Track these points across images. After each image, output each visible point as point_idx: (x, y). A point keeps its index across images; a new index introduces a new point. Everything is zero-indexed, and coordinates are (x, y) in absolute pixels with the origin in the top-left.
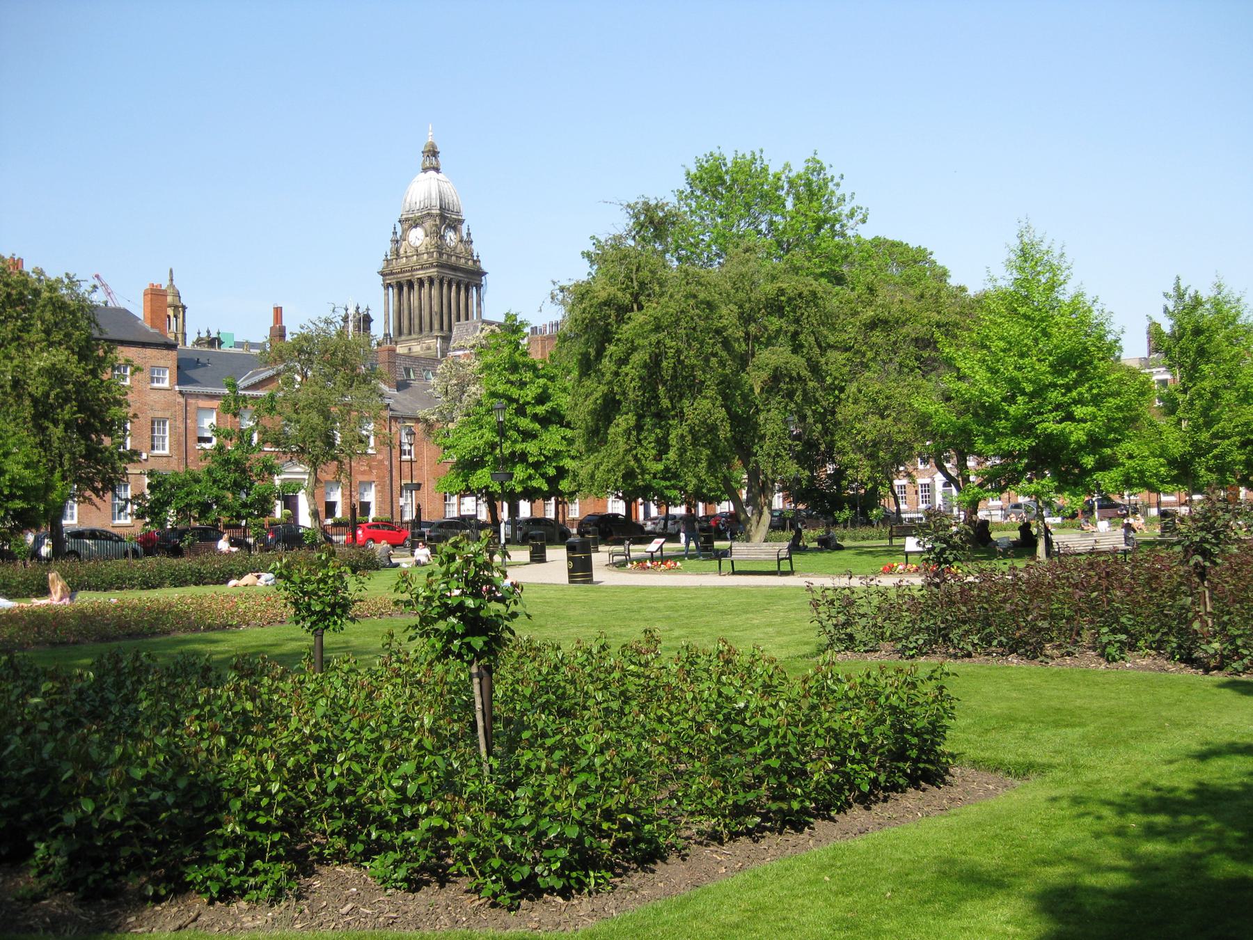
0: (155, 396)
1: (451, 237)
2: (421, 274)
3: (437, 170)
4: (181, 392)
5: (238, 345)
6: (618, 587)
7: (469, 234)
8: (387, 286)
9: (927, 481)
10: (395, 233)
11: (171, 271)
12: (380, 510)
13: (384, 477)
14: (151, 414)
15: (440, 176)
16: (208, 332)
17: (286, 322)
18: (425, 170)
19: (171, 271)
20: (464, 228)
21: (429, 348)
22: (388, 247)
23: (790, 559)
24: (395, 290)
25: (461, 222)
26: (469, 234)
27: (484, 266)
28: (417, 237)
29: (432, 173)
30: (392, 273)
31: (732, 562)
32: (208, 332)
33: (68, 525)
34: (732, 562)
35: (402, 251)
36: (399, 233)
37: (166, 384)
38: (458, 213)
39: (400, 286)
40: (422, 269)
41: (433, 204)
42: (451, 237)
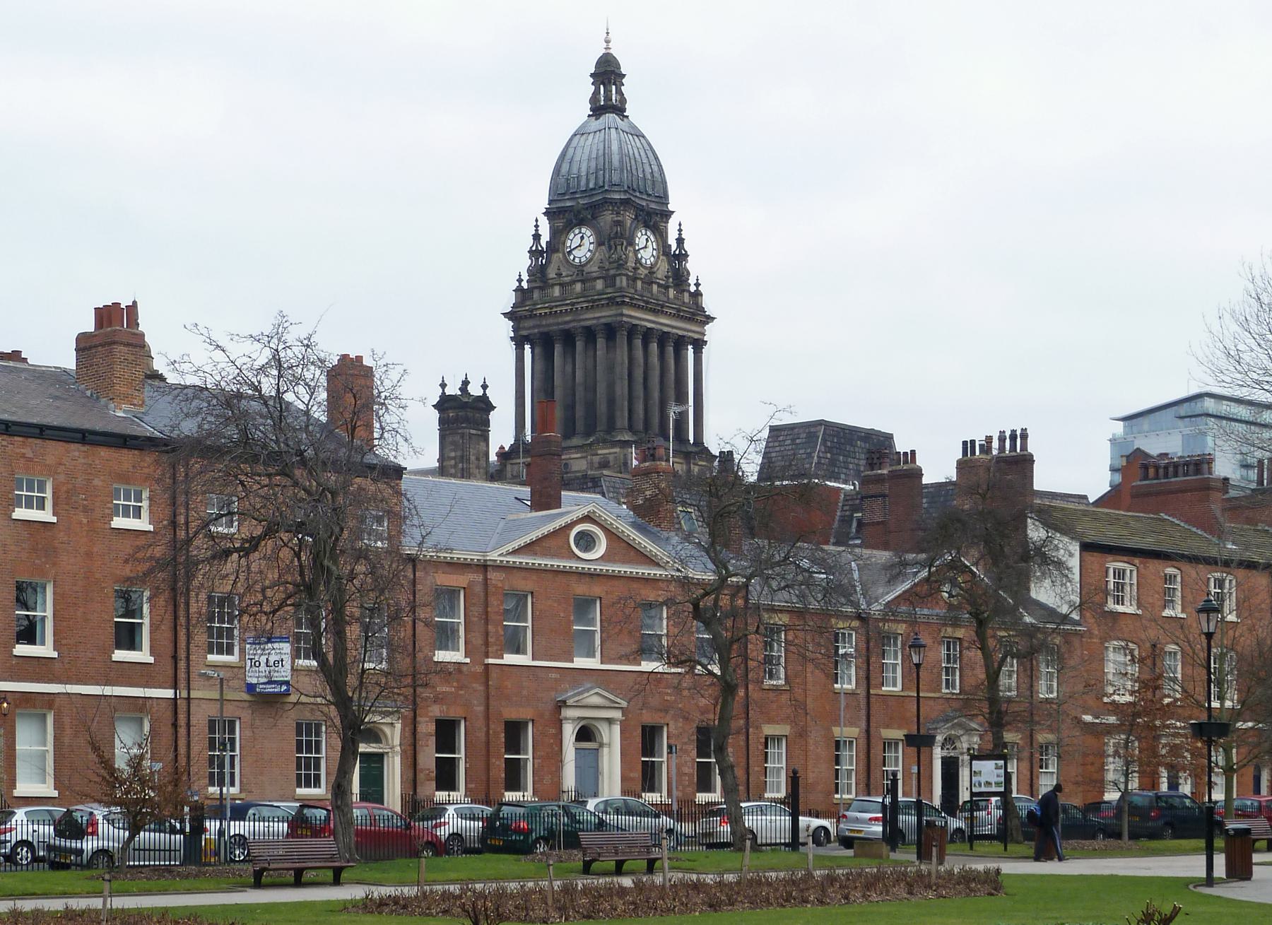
1: (645, 247)
10: (537, 237)
25: (668, 214)
28: (582, 245)
35: (552, 273)
36: (545, 237)
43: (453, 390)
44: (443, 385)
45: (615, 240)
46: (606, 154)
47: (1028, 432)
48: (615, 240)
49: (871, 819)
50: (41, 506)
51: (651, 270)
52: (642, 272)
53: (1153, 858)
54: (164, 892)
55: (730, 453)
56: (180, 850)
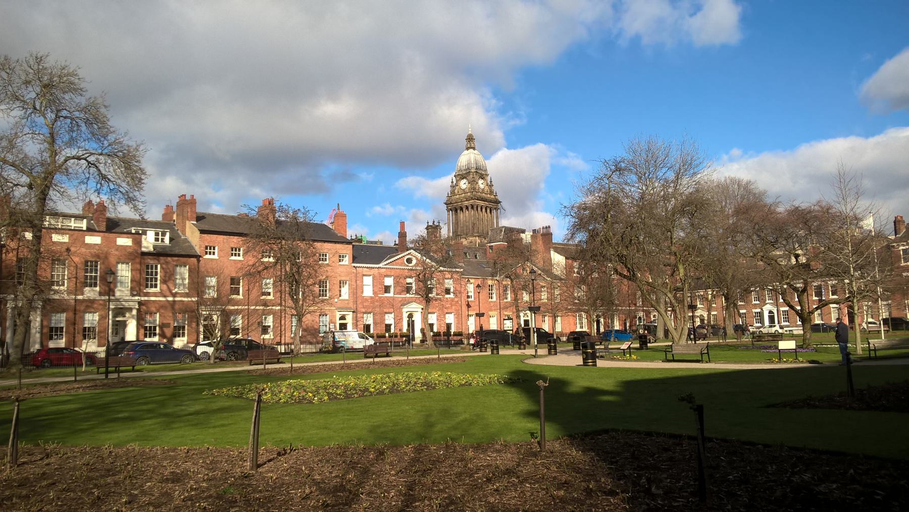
0: (340, 269)
1: (481, 184)
2: (466, 203)
3: (474, 149)
4: (354, 267)
5: (368, 242)
6: (659, 369)
7: (491, 182)
8: (448, 210)
9: (759, 310)
10: (452, 182)
11: (338, 204)
12: (457, 327)
13: (459, 310)
14: (339, 279)
15: (476, 152)
16: (356, 236)
17: (407, 230)
18: (468, 149)
19: (338, 204)
20: (488, 179)
21: (471, 242)
22: (449, 190)
23: (708, 353)
24: (454, 212)
25: (487, 175)
26: (491, 182)
27: (499, 198)
28: (464, 184)
29: (471, 150)
30: (451, 203)
31: (673, 355)
32: (356, 236)
33: (637, 343)
34: (673, 355)
35: (456, 191)
36: (455, 182)
37: (347, 263)
38: (486, 170)
39: (456, 210)
40: (467, 201)
41: (472, 166)
42: (481, 184)
43: (431, 224)
44: (428, 223)
45: (473, 182)
46: (469, 160)
47: (552, 231)
48: (473, 182)
49: (342, 367)
50: (239, 255)
51: (483, 190)
52: (481, 190)
53: (647, 377)
54: (652, 360)
55: (119, 225)
56: (133, 370)
